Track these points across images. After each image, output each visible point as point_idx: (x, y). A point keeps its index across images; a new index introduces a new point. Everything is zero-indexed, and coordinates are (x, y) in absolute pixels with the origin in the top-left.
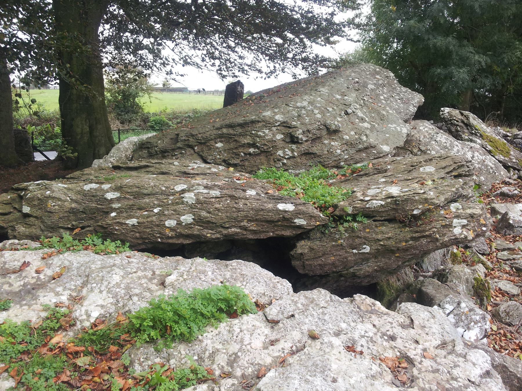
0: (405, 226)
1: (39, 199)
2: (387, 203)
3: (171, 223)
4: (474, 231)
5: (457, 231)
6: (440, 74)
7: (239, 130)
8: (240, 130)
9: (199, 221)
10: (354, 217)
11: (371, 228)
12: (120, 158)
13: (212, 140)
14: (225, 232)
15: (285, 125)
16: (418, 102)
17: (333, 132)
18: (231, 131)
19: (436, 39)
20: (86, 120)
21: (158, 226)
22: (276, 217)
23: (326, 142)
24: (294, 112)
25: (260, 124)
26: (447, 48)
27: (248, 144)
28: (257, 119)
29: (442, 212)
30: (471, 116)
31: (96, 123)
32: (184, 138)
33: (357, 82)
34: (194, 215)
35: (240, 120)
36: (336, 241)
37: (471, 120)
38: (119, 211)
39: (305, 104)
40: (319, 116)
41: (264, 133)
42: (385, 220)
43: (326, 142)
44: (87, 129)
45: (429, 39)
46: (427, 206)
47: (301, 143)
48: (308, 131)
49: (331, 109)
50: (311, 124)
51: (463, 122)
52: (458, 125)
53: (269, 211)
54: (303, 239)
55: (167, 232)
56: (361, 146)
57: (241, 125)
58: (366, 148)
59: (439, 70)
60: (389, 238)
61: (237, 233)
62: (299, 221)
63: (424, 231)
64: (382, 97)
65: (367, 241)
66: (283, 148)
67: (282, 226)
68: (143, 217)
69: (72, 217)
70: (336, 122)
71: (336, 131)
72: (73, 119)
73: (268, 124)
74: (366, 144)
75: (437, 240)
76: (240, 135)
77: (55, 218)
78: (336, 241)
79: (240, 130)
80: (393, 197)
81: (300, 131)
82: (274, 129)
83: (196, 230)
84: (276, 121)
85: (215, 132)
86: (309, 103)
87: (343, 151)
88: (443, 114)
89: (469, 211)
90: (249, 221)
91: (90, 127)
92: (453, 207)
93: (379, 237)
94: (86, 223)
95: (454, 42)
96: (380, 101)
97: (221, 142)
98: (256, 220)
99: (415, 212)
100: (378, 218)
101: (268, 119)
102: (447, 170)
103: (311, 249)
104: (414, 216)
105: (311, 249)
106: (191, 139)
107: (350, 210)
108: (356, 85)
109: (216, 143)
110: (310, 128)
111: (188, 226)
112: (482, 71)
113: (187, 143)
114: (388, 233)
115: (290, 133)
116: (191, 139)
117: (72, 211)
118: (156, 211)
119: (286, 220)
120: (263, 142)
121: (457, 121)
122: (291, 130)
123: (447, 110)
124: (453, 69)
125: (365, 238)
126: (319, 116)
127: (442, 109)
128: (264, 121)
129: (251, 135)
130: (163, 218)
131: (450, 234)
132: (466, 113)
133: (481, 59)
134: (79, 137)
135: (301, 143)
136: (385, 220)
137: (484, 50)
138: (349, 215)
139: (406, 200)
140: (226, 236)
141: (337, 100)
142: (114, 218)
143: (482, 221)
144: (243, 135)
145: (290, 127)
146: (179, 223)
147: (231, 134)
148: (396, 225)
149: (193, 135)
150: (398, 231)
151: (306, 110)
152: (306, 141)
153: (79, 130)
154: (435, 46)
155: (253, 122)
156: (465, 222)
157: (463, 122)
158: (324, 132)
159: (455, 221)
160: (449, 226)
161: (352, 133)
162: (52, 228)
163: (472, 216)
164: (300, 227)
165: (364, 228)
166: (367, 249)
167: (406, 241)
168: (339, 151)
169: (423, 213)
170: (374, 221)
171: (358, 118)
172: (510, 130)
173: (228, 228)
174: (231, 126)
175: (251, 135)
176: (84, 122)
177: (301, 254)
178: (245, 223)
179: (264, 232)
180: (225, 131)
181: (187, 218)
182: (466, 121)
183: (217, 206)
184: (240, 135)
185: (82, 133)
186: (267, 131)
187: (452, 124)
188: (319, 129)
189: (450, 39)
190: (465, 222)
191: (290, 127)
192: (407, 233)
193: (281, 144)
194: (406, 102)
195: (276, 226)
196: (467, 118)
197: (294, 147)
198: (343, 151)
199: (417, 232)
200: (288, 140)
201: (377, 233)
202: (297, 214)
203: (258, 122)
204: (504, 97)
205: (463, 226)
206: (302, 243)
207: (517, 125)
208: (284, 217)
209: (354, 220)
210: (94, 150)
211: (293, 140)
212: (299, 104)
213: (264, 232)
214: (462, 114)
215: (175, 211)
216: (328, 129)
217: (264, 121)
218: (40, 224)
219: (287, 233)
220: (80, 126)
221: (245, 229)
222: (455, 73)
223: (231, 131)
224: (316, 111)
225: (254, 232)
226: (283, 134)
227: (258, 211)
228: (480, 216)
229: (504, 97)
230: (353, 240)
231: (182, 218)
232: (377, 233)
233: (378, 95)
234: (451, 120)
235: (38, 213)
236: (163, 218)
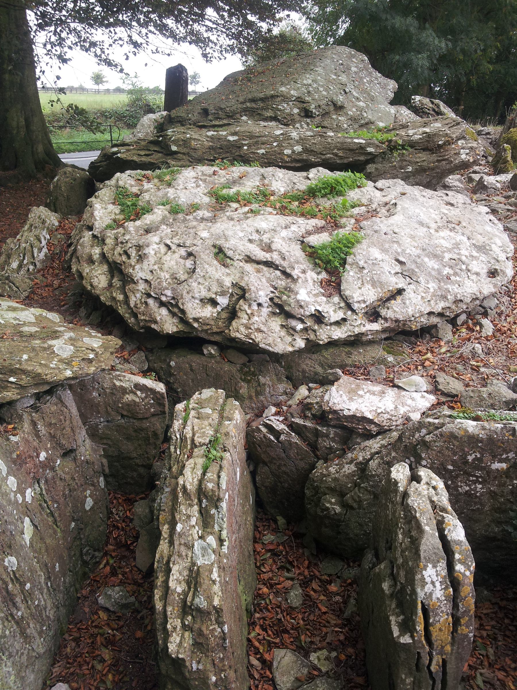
0: (433, 153)
1: (183, 140)
2: (423, 137)
3: (287, 152)
4: (473, 157)
5: (463, 156)
6: (398, 61)
7: (261, 104)
8: (262, 105)
9: (306, 150)
10: (403, 147)
11: (413, 155)
12: (148, 133)
13: (238, 113)
14: (323, 157)
15: (300, 100)
16: (393, 88)
17: (339, 108)
18: (254, 105)
19: (394, 19)
20: (21, 112)
21: (279, 154)
22: (355, 147)
23: (334, 117)
24: (303, 89)
25: (279, 99)
26: (407, 31)
27: (271, 117)
28: (276, 94)
29: (453, 146)
30: (441, 104)
31: (32, 116)
32: (213, 111)
33: (342, 64)
34: (302, 146)
35: (262, 95)
36: (392, 163)
37: (442, 108)
38: (249, 145)
39: (310, 82)
40: (324, 93)
41: (283, 107)
42: (421, 149)
43: (334, 117)
44: (23, 122)
45: (386, 19)
46: (447, 139)
47: (314, 117)
48: (319, 106)
49: (332, 88)
50: (320, 100)
51: (434, 110)
52: (429, 113)
53: (350, 143)
54: (369, 163)
55: (286, 158)
56: (362, 122)
57: (262, 100)
58: (367, 124)
59: (397, 57)
60: (424, 161)
61: (331, 158)
62: (370, 150)
63: (445, 156)
64: (365, 81)
65: (410, 163)
66: (300, 122)
67: (358, 153)
68: (268, 148)
69: (212, 152)
70: (340, 99)
71: (341, 108)
72: (7, 110)
73: (286, 98)
74: (366, 120)
75: (452, 162)
76: (262, 109)
77: (200, 153)
78: (392, 163)
79: (262, 105)
80: (427, 133)
81: (313, 106)
82: (291, 103)
83: (305, 156)
84: (293, 96)
85: (240, 106)
86: (313, 81)
87: (349, 126)
88: (414, 103)
89: (470, 145)
90: (338, 150)
91: (26, 120)
92: (460, 143)
93: (418, 160)
94: (224, 156)
95: (416, 23)
96: (364, 84)
97: (246, 115)
98: (343, 149)
99: (440, 143)
100: (418, 148)
101: (285, 94)
102: (449, 126)
103: (377, 169)
104: (439, 145)
105: (377, 169)
106: (220, 113)
107: (400, 142)
108: (341, 67)
109: (242, 116)
110: (321, 103)
111: (300, 153)
112: (442, 58)
113: (216, 116)
114: (423, 157)
115: (304, 108)
116: (220, 113)
117: (211, 148)
118: (275, 144)
119: (361, 148)
120: (283, 115)
121: (429, 110)
122: (305, 105)
123: (418, 98)
124: (412, 55)
125: (409, 161)
126: (324, 93)
127: (413, 97)
128: (282, 96)
129: (273, 109)
130: (282, 148)
131: (459, 159)
132: (437, 101)
133: (442, 45)
134: (15, 132)
135: (314, 117)
136: (421, 149)
137: (443, 32)
138: (399, 145)
139: (435, 135)
140: (323, 160)
141: (334, 79)
142: (247, 150)
143: (477, 152)
144: (265, 109)
145: (303, 102)
146: (294, 151)
147: (254, 108)
148: (428, 153)
149: (221, 109)
150: (429, 156)
151: (312, 87)
152: (318, 116)
153: (14, 124)
154: (393, 28)
155: (273, 97)
156: (468, 151)
157: (434, 110)
158: (332, 108)
159: (462, 150)
160: (458, 154)
161: (354, 110)
162: (199, 160)
163: (472, 148)
164: (370, 153)
165: (409, 154)
166: (410, 169)
167: (434, 163)
168: (345, 126)
169: (444, 144)
170: (416, 149)
171: (354, 97)
172: (473, 127)
173: (325, 154)
174: (253, 100)
175: (273, 109)
176: (19, 114)
177: (370, 173)
178: (335, 151)
179: (347, 158)
180: (248, 104)
181: (298, 148)
182: (437, 109)
183: (313, 141)
184: (262, 109)
185: (18, 127)
186: (285, 105)
187: (423, 112)
188: (328, 105)
189: (409, 20)
190: (468, 151)
191: (303, 102)
192: (434, 157)
193: (297, 118)
194: (384, 87)
195: (355, 153)
196: (438, 106)
197: (308, 120)
198: (349, 126)
199: (440, 156)
200: (302, 114)
201: (416, 158)
202: (369, 145)
203: (277, 96)
204: (463, 93)
205: (467, 154)
206: (370, 165)
207: (481, 120)
208: (360, 146)
209: (403, 148)
210: (32, 147)
211: (307, 114)
212: (305, 82)
213: (347, 158)
214: (433, 103)
215: (289, 143)
216: (335, 105)
217: (282, 96)
218: (188, 158)
219: (362, 158)
220: (16, 119)
221: (336, 155)
222: (415, 61)
223: (254, 105)
224: (321, 89)
225: (341, 158)
226: (299, 108)
227: (342, 143)
228: (476, 148)
229: (463, 93)
230: (402, 163)
231: (295, 148)
232: (416, 158)
233: (361, 78)
234: (422, 108)
235: (185, 150)
236: (282, 148)
